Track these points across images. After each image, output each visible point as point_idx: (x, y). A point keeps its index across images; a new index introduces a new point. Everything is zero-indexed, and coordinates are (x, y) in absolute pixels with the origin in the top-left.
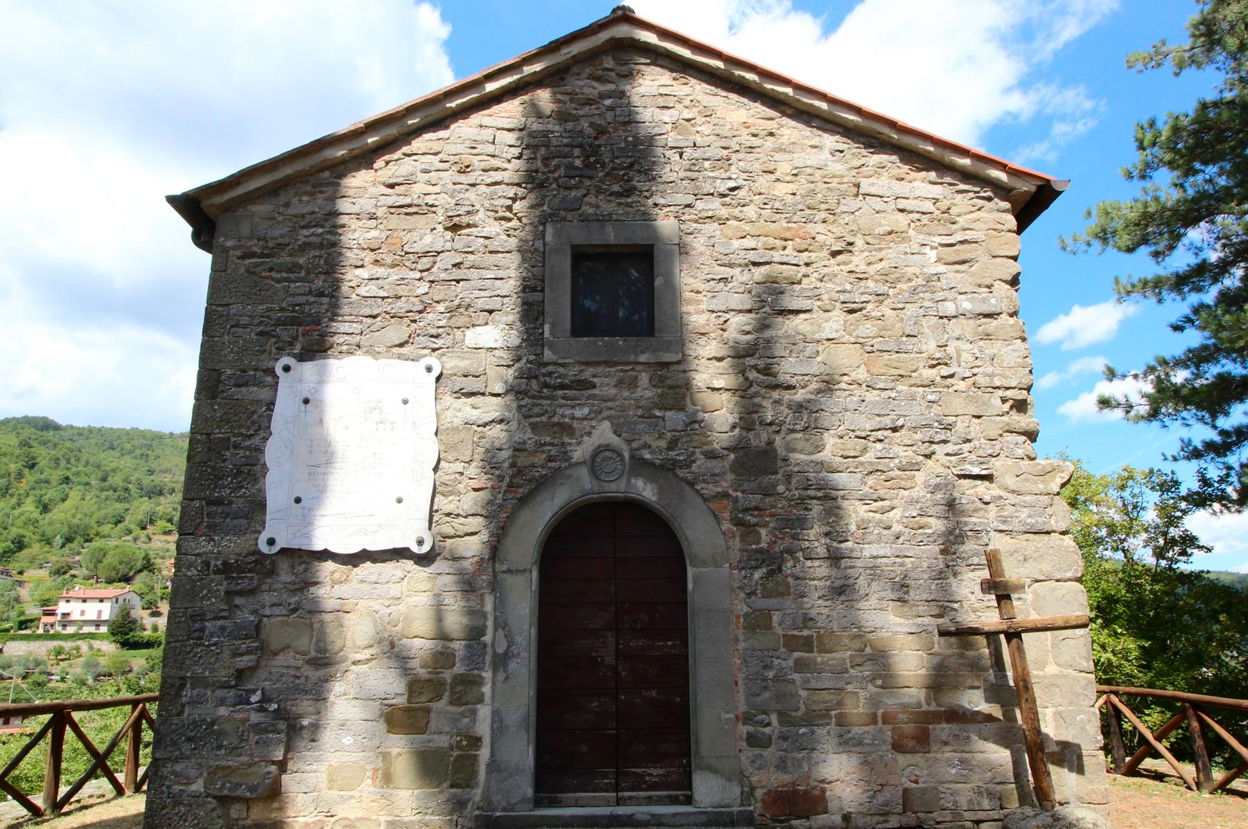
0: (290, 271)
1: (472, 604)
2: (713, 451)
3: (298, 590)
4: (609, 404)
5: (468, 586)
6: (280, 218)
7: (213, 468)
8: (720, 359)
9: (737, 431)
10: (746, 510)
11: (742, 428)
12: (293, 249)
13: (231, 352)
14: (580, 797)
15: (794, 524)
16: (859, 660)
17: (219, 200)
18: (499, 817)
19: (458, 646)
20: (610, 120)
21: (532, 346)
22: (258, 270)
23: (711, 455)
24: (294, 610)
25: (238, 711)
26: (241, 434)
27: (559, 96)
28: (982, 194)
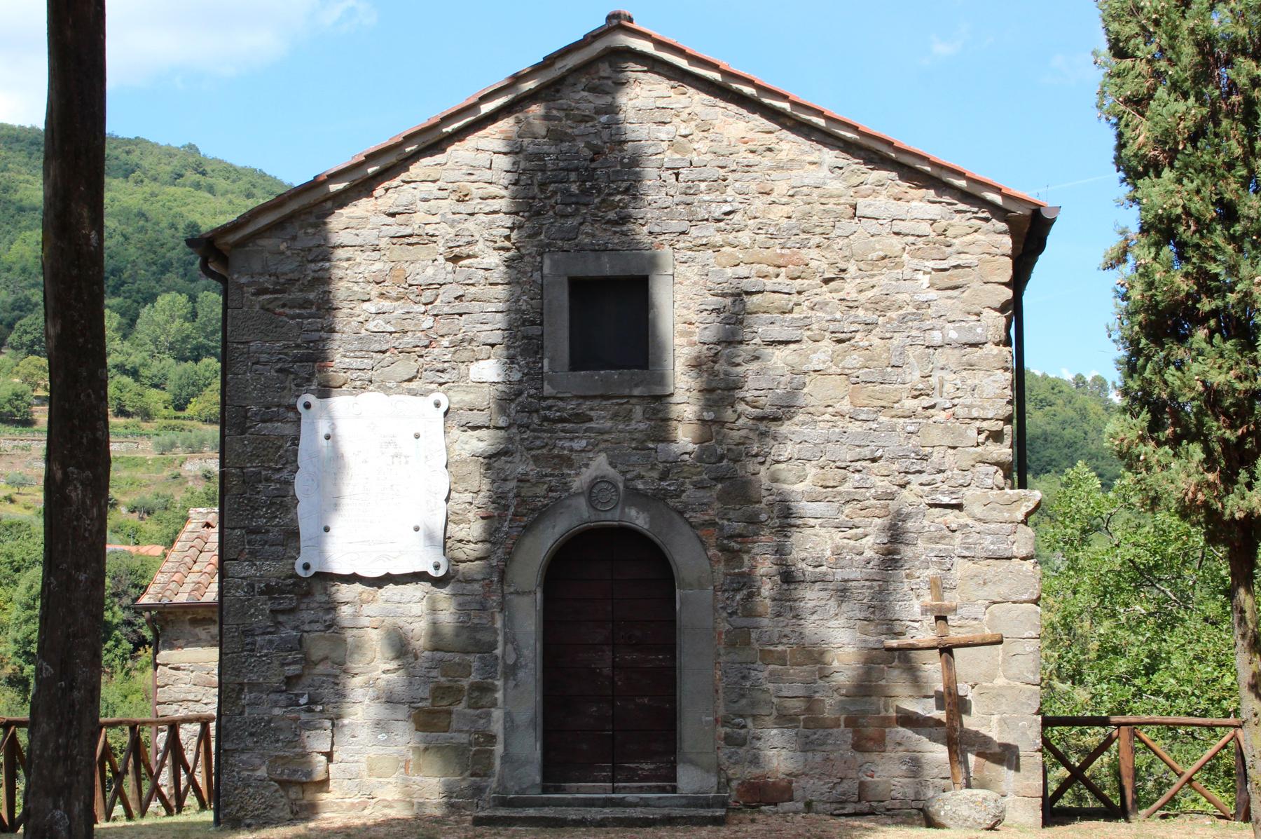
0: (301, 307)
4: (606, 437)
7: (249, 500)
26: (270, 468)
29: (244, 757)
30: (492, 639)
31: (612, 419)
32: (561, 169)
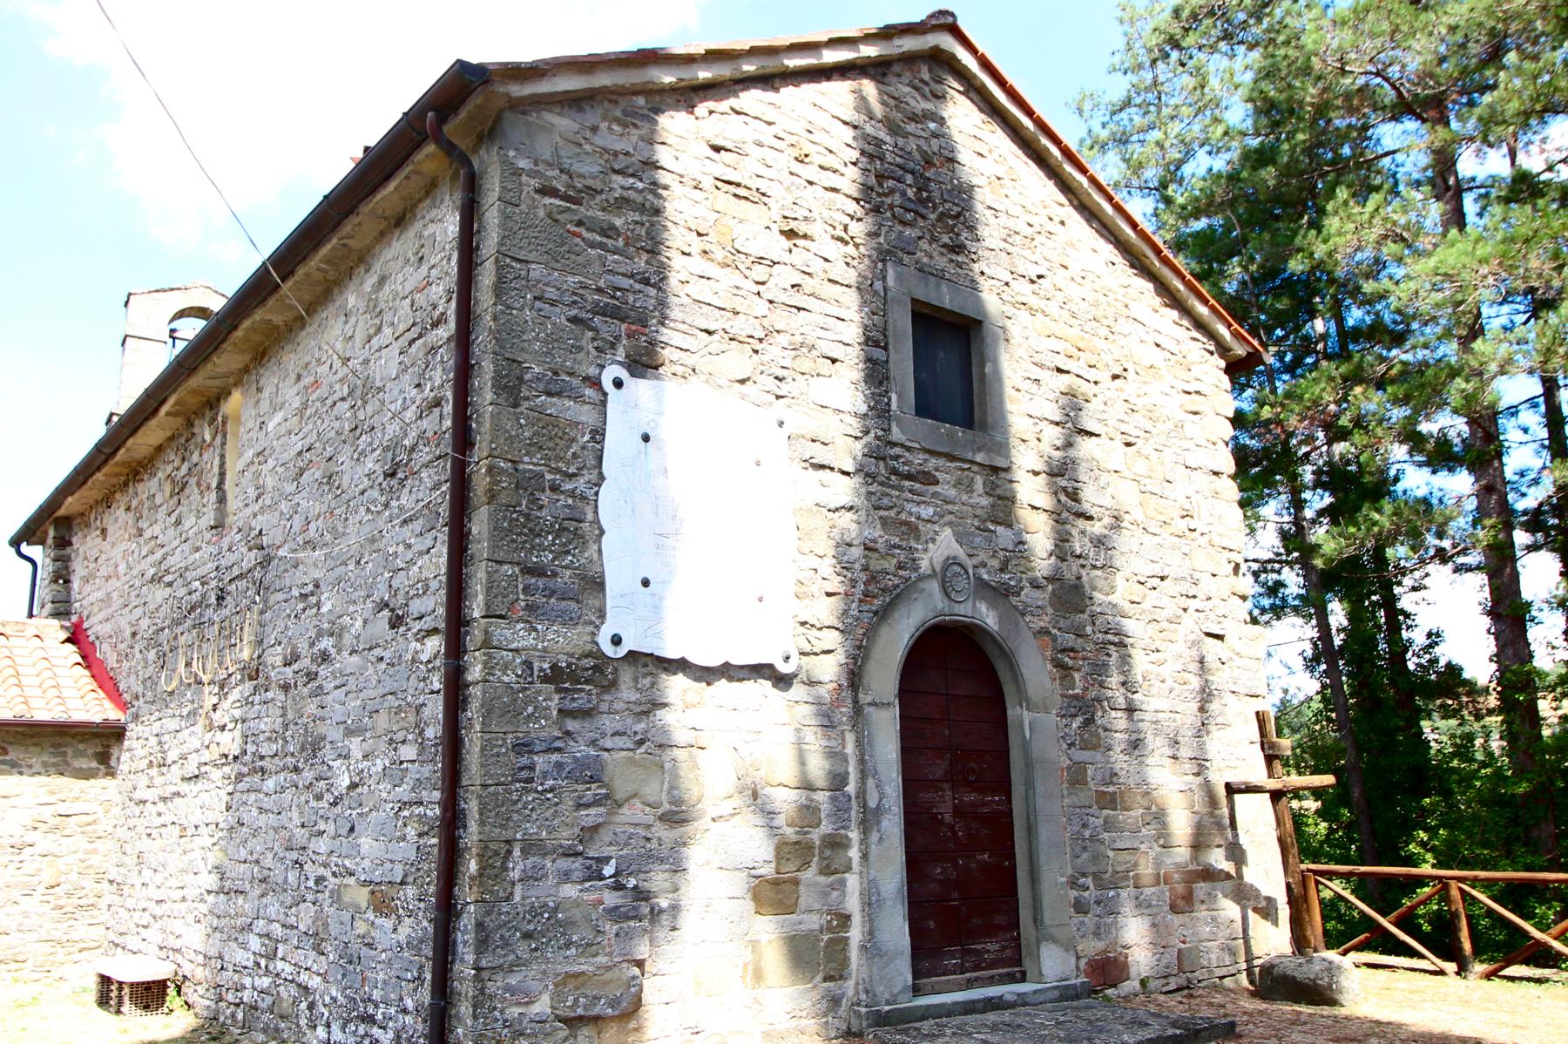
0: (604, 233)
1: (833, 743)
2: (1035, 579)
3: (643, 713)
4: (950, 507)
5: (827, 722)
6: (587, 147)
7: (527, 517)
8: (1036, 473)
9: (1053, 558)
10: (1063, 651)
11: (1058, 557)
12: (607, 201)
13: (537, 339)
14: (937, 982)
15: (1099, 671)
16: (1148, 819)
17: (519, 90)
18: (888, 1012)
19: (822, 797)
20: (936, 149)
21: (879, 417)
22: (561, 217)
23: (1036, 585)
24: (641, 743)
25: (588, 890)
26: (558, 471)
27: (886, 97)
28: (1207, 347)
29: (513, 980)
30: (843, 770)
31: (954, 486)
32: (897, 166)
